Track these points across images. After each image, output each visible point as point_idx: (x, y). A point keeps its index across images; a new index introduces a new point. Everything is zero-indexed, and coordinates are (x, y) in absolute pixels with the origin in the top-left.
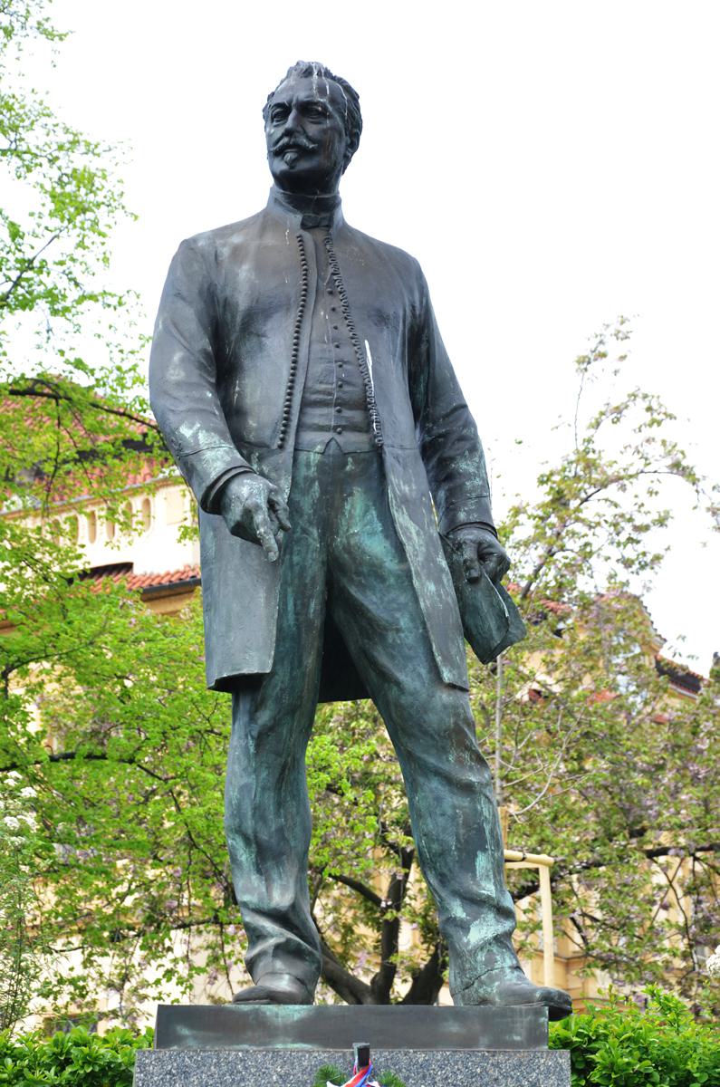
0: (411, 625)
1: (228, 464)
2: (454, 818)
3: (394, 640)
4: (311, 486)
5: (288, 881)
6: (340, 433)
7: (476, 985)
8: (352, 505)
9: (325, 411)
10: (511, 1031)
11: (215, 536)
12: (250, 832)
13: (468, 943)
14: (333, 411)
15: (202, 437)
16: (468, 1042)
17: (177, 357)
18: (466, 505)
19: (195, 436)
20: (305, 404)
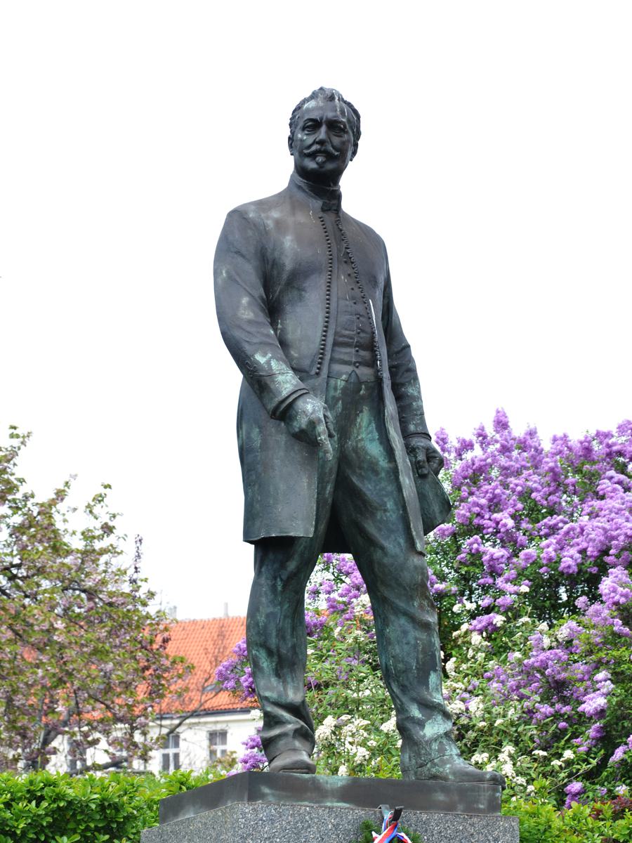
0: (395, 507)
1: (295, 386)
2: (416, 646)
3: (382, 517)
4: (336, 404)
5: (298, 683)
6: (357, 367)
7: (429, 765)
8: (362, 420)
9: (348, 350)
10: (478, 802)
11: (260, 432)
12: (273, 647)
13: (425, 735)
14: (353, 350)
15: (274, 364)
16: (449, 808)
17: (245, 300)
18: (413, 419)
19: (268, 362)
20: (335, 344)
